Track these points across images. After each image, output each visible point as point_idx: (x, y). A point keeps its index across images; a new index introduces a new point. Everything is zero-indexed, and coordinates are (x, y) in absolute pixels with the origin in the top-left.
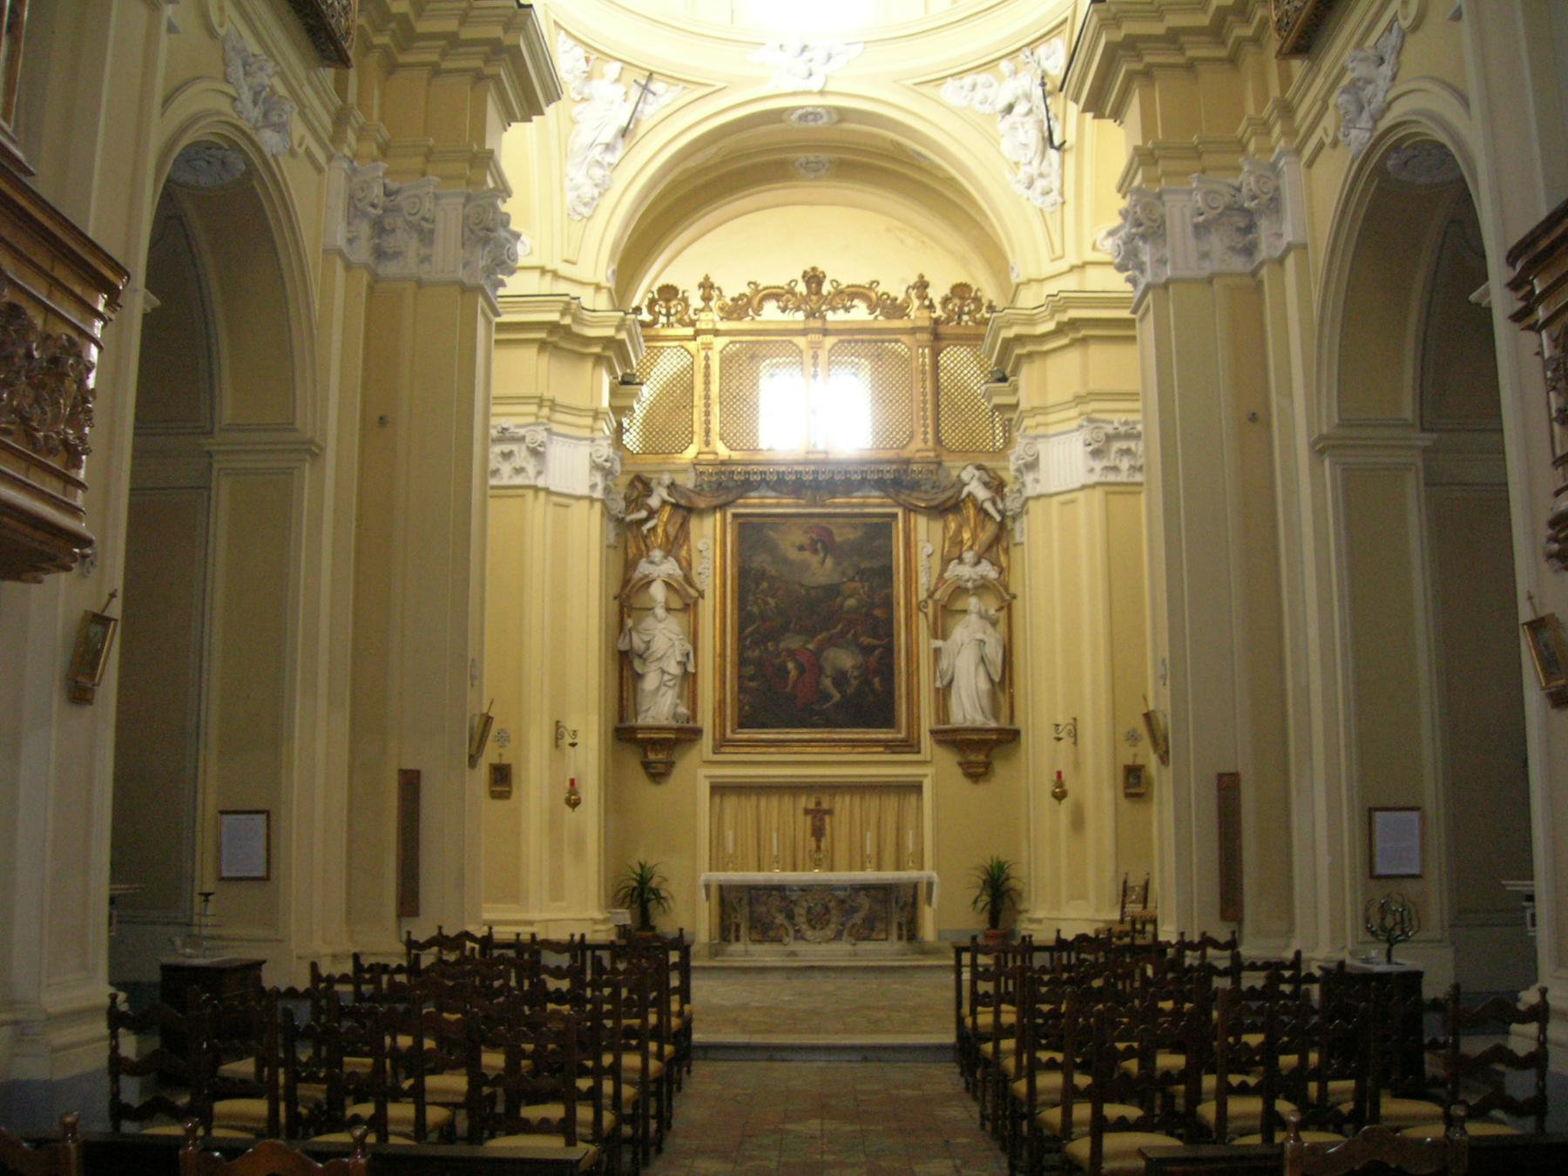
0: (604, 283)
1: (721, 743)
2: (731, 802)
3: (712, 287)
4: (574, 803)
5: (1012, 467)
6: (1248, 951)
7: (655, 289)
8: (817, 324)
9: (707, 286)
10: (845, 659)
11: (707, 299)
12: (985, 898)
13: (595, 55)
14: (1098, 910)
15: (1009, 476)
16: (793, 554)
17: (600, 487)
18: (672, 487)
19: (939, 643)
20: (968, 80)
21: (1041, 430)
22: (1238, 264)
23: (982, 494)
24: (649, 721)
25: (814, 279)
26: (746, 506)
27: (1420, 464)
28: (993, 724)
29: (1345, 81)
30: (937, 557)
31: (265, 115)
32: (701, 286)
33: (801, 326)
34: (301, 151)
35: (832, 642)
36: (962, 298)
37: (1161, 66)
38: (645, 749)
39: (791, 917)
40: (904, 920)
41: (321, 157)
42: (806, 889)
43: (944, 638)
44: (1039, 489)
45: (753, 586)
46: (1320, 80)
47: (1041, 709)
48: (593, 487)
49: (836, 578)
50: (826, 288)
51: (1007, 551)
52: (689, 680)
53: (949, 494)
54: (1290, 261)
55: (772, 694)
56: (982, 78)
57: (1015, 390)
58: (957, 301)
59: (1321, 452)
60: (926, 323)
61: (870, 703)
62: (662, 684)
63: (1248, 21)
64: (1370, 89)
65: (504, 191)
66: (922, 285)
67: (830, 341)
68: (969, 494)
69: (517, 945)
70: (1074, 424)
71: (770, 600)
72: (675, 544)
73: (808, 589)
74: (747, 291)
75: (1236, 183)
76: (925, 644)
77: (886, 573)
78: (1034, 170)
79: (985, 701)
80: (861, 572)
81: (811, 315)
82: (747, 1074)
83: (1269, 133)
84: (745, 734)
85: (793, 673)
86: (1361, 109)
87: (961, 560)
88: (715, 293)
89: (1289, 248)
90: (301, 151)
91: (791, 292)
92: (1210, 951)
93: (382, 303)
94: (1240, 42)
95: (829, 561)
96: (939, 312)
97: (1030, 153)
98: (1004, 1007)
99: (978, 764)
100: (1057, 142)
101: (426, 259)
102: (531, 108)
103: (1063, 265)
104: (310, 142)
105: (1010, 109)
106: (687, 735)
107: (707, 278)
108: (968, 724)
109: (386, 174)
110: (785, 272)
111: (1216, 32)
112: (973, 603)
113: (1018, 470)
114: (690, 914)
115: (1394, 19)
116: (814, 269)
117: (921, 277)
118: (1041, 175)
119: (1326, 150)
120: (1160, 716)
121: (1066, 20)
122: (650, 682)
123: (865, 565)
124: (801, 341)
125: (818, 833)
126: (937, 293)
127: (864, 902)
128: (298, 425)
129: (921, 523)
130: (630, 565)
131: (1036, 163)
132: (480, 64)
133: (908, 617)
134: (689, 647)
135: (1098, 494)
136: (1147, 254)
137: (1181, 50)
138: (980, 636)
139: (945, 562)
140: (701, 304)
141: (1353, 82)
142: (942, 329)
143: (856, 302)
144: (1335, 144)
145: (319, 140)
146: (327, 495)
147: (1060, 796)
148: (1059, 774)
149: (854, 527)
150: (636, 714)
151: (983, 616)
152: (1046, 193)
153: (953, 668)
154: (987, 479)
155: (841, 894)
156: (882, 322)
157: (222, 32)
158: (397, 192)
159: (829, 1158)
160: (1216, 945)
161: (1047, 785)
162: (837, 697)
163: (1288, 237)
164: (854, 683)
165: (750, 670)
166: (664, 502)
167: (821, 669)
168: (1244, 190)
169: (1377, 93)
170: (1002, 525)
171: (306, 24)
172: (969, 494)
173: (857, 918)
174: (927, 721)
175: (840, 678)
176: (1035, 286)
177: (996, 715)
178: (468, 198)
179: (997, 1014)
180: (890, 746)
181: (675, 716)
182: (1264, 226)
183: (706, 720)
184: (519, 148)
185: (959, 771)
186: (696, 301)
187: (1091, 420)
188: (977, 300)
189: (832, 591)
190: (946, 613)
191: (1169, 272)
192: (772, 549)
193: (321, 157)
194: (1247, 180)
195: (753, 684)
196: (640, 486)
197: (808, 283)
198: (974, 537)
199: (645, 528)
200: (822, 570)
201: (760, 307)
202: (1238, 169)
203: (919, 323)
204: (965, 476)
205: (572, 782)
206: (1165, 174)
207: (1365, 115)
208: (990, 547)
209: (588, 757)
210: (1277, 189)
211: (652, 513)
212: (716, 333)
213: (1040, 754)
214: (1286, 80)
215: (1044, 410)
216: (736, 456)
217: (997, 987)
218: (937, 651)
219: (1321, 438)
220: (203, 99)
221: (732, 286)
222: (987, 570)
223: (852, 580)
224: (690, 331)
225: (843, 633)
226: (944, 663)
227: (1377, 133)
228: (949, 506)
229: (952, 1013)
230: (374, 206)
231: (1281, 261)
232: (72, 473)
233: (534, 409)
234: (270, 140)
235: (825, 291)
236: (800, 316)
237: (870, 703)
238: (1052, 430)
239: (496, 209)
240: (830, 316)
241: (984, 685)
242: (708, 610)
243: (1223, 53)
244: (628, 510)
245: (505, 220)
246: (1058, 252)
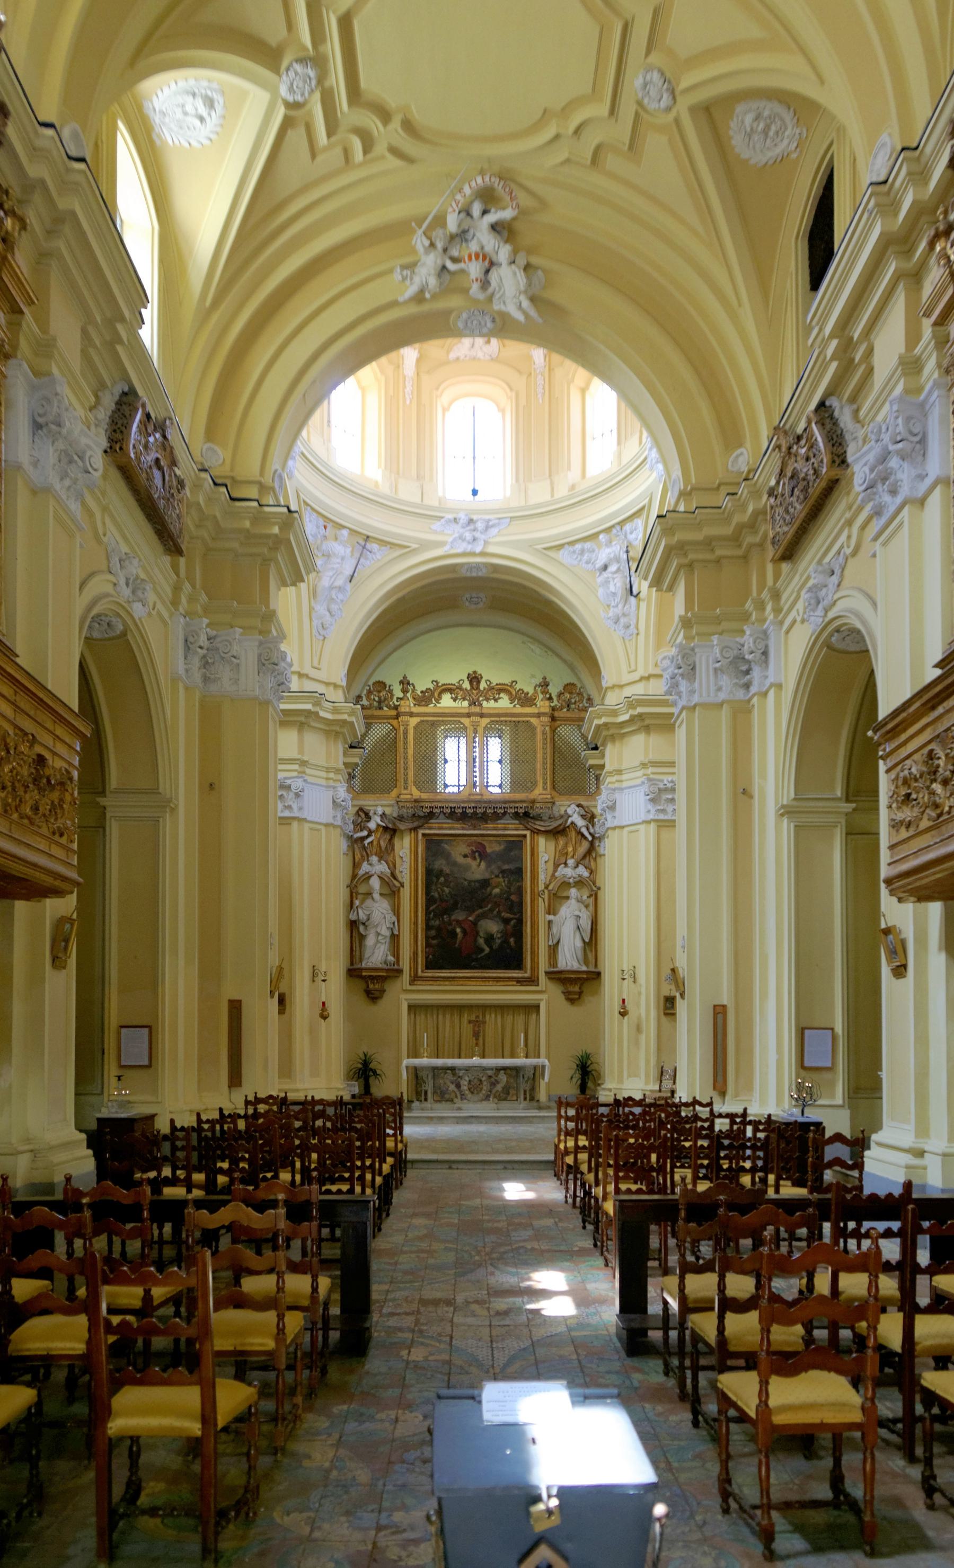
0: (339, 683)
1: (415, 979)
2: (421, 1019)
3: (408, 683)
4: (324, 1017)
5: (599, 808)
6: (717, 1108)
7: (371, 683)
8: (476, 709)
9: (405, 683)
10: (492, 927)
11: (405, 691)
12: (578, 1076)
13: (330, 523)
14: (647, 1083)
15: (598, 811)
16: (460, 860)
17: (339, 818)
18: (383, 816)
19: (551, 917)
20: (578, 546)
21: (617, 785)
22: (740, 694)
23: (580, 822)
24: (370, 965)
25: (474, 679)
26: (430, 828)
27: (844, 823)
28: (584, 968)
29: (810, 584)
30: (551, 864)
31: (133, 592)
32: (401, 682)
33: (467, 711)
34: (154, 613)
35: (483, 916)
36: (571, 693)
37: (697, 561)
38: (368, 983)
39: (458, 1086)
40: (528, 1089)
41: (166, 615)
42: (467, 1069)
43: (555, 914)
44: (616, 823)
45: (434, 879)
46: (797, 578)
47: (612, 963)
48: (334, 817)
49: (487, 876)
50: (483, 685)
51: (595, 859)
52: (395, 939)
53: (560, 822)
54: (771, 694)
55: (448, 949)
56: (588, 545)
57: (603, 756)
58: (568, 695)
59: (782, 815)
60: (547, 710)
61: (508, 955)
62: (378, 942)
63: (756, 532)
64: (824, 590)
65: (282, 636)
66: (545, 684)
67: (485, 721)
68: (572, 823)
69: (303, 1103)
70: (638, 781)
71: (447, 890)
72: (386, 854)
73: (470, 882)
74: (431, 686)
75: (742, 641)
76: (543, 918)
77: (519, 872)
78: (619, 610)
79: (580, 954)
80: (503, 872)
81: (472, 703)
82: (437, 1176)
83: (764, 609)
84: (430, 973)
85: (460, 935)
86: (818, 602)
87: (566, 864)
88: (410, 688)
89: (772, 685)
90: (154, 613)
91: (460, 688)
92: (698, 1108)
93: (210, 716)
94: (751, 546)
95: (483, 864)
96: (555, 703)
97: (617, 599)
98: (580, 1137)
99: (575, 993)
100: (635, 592)
101: (236, 681)
102: (298, 578)
103: (636, 676)
104: (159, 606)
105: (605, 567)
106: (394, 972)
107: (405, 677)
108: (568, 968)
109: (208, 625)
110: (456, 675)
111: (735, 539)
112: (573, 892)
113: (603, 810)
114: (393, 1083)
115: (842, 547)
116: (475, 672)
117: (545, 678)
118: (624, 615)
119: (798, 624)
120: (680, 971)
121: (642, 509)
122: (370, 941)
123: (506, 867)
124: (466, 721)
125: (476, 1035)
126: (554, 690)
127: (503, 1077)
128: (161, 790)
129: (541, 841)
130: (356, 866)
131: (620, 606)
132: (266, 550)
133: (532, 901)
134: (395, 919)
135: (653, 826)
136: (684, 686)
137: (712, 550)
138: (577, 913)
139: (556, 866)
140: (401, 695)
141: (815, 586)
142: (556, 714)
143: (502, 695)
144: (803, 621)
145: (163, 603)
146: (180, 835)
147: (623, 1014)
148: (624, 1001)
149: (499, 843)
150: (361, 961)
151: (579, 901)
152: (627, 627)
153: (560, 932)
154: (583, 812)
155: (490, 1073)
156: (519, 709)
157: (105, 539)
158: (215, 637)
159: (486, 1218)
160: (701, 1104)
161: (617, 1007)
162: (487, 950)
163: (771, 679)
164: (498, 941)
165: (433, 933)
166: (378, 825)
167: (477, 933)
168: (746, 647)
169: (828, 595)
170: (592, 843)
171: (154, 528)
172: (572, 823)
173: (499, 1087)
174: (543, 966)
175: (490, 939)
176: (617, 690)
177: (586, 962)
178: (261, 643)
179: (576, 1141)
180: (520, 981)
181: (385, 962)
182: (756, 673)
183: (405, 964)
184: (287, 602)
185: (562, 997)
186: (398, 693)
187: (649, 780)
188: (580, 694)
189: (485, 883)
190: (557, 898)
191: (696, 699)
192: (447, 856)
193: (166, 615)
194: (748, 640)
195: (434, 942)
196: (363, 815)
197: (471, 683)
198: (575, 850)
199: (366, 842)
200: (477, 870)
201: (440, 697)
202: (742, 632)
203: (542, 710)
204: (570, 811)
205: (324, 1004)
206: (697, 634)
207: (820, 606)
208: (584, 857)
209: (335, 988)
210: (767, 646)
211: (370, 833)
212: (412, 715)
213: (612, 988)
214: (777, 576)
215: (619, 772)
216: (424, 796)
217: (577, 1125)
218: (550, 922)
219: (783, 806)
220: (99, 585)
221: (422, 684)
222: (582, 871)
223: (497, 876)
224: (394, 713)
225: (491, 910)
226: (555, 930)
227: (827, 620)
228: (559, 831)
229: (861, 1466)
230: (201, 647)
231: (765, 694)
232: (70, 846)
233: (296, 767)
234: (138, 610)
235: (482, 688)
236: (466, 704)
237: (508, 955)
238: (625, 784)
239: (278, 649)
240: (485, 704)
241: (579, 944)
242: (406, 895)
243: (740, 552)
244: (355, 831)
245: (283, 656)
246: (633, 667)
